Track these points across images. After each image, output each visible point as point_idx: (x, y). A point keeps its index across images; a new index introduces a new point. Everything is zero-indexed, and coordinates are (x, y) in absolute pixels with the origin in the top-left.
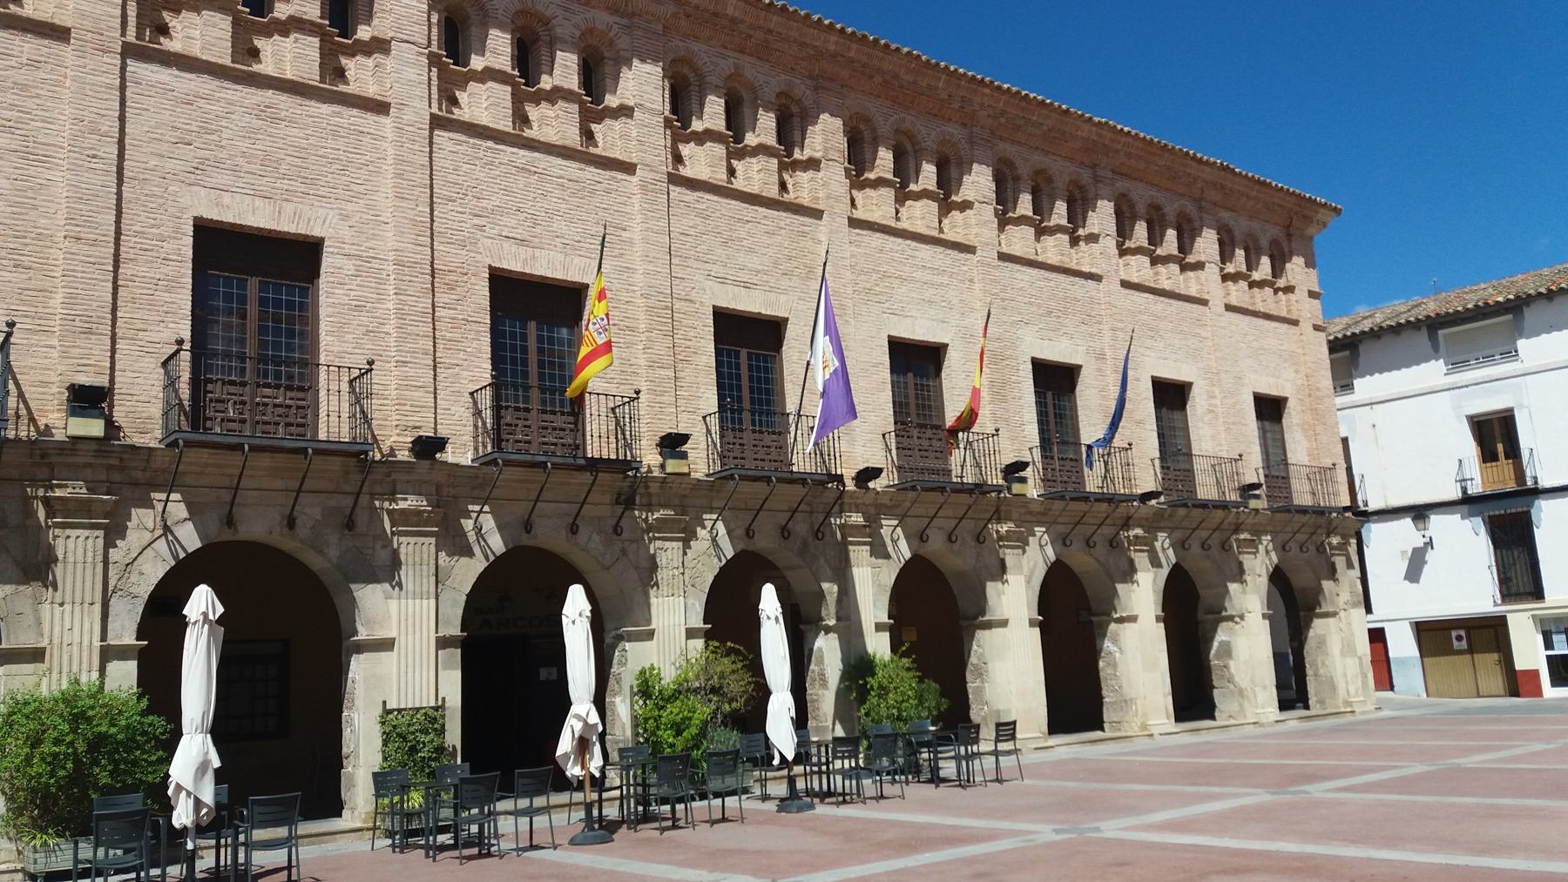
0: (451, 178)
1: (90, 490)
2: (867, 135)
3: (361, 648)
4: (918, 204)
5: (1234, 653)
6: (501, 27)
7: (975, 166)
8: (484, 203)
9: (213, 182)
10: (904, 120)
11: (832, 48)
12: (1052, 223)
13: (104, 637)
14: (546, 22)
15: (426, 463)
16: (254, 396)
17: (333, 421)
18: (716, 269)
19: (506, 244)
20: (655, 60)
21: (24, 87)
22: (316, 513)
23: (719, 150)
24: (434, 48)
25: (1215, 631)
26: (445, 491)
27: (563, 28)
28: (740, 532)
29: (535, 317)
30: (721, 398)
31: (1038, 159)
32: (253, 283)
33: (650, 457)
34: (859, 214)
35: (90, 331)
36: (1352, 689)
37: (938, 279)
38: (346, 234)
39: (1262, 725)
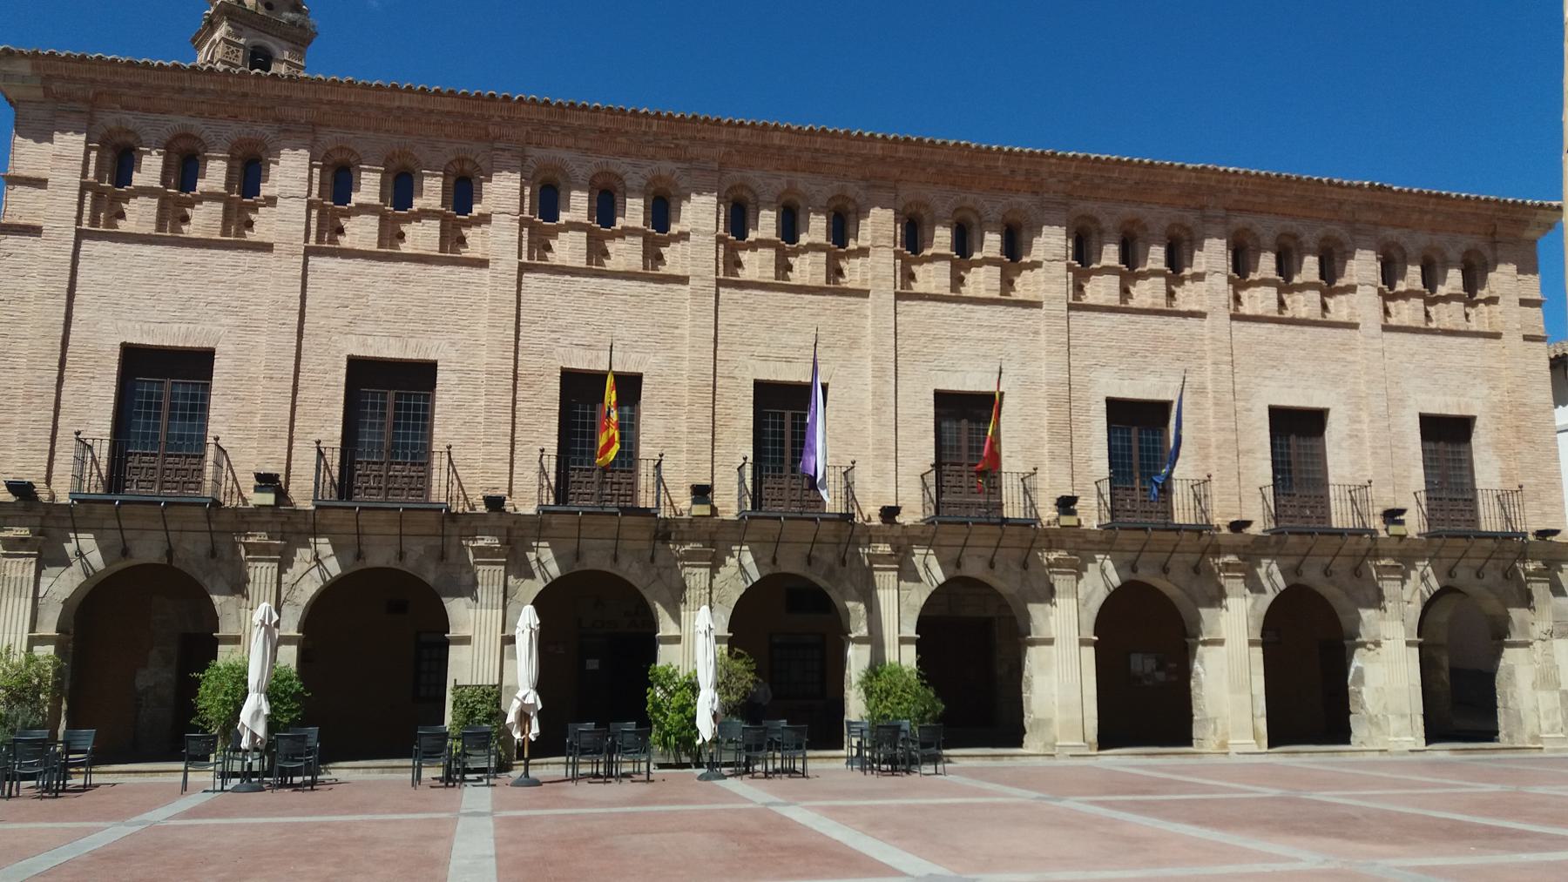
0: (536, 306)
1: (270, 538)
2: (1397, 255)
3: (1033, 643)
4: (982, 270)
5: (1366, 679)
6: (580, 188)
7: (1045, 229)
8: (560, 322)
9: (361, 330)
10: (965, 199)
11: (879, 152)
12: (415, 208)
13: (33, 628)
14: (1094, 220)
15: (495, 514)
16: (388, 470)
17: (1183, 512)
18: (761, 350)
19: (576, 350)
20: (711, 192)
21: (245, 285)
22: (420, 549)
23: (1419, 303)
24: (526, 215)
25: (1352, 657)
26: (515, 533)
27: (633, 180)
28: (768, 560)
29: (1141, 430)
30: (1275, 471)
31: (1127, 211)
32: (391, 394)
33: (1376, 523)
34: (1393, 321)
35: (275, 437)
36: (1545, 725)
37: (993, 335)
38: (453, 355)
39: (1391, 754)
